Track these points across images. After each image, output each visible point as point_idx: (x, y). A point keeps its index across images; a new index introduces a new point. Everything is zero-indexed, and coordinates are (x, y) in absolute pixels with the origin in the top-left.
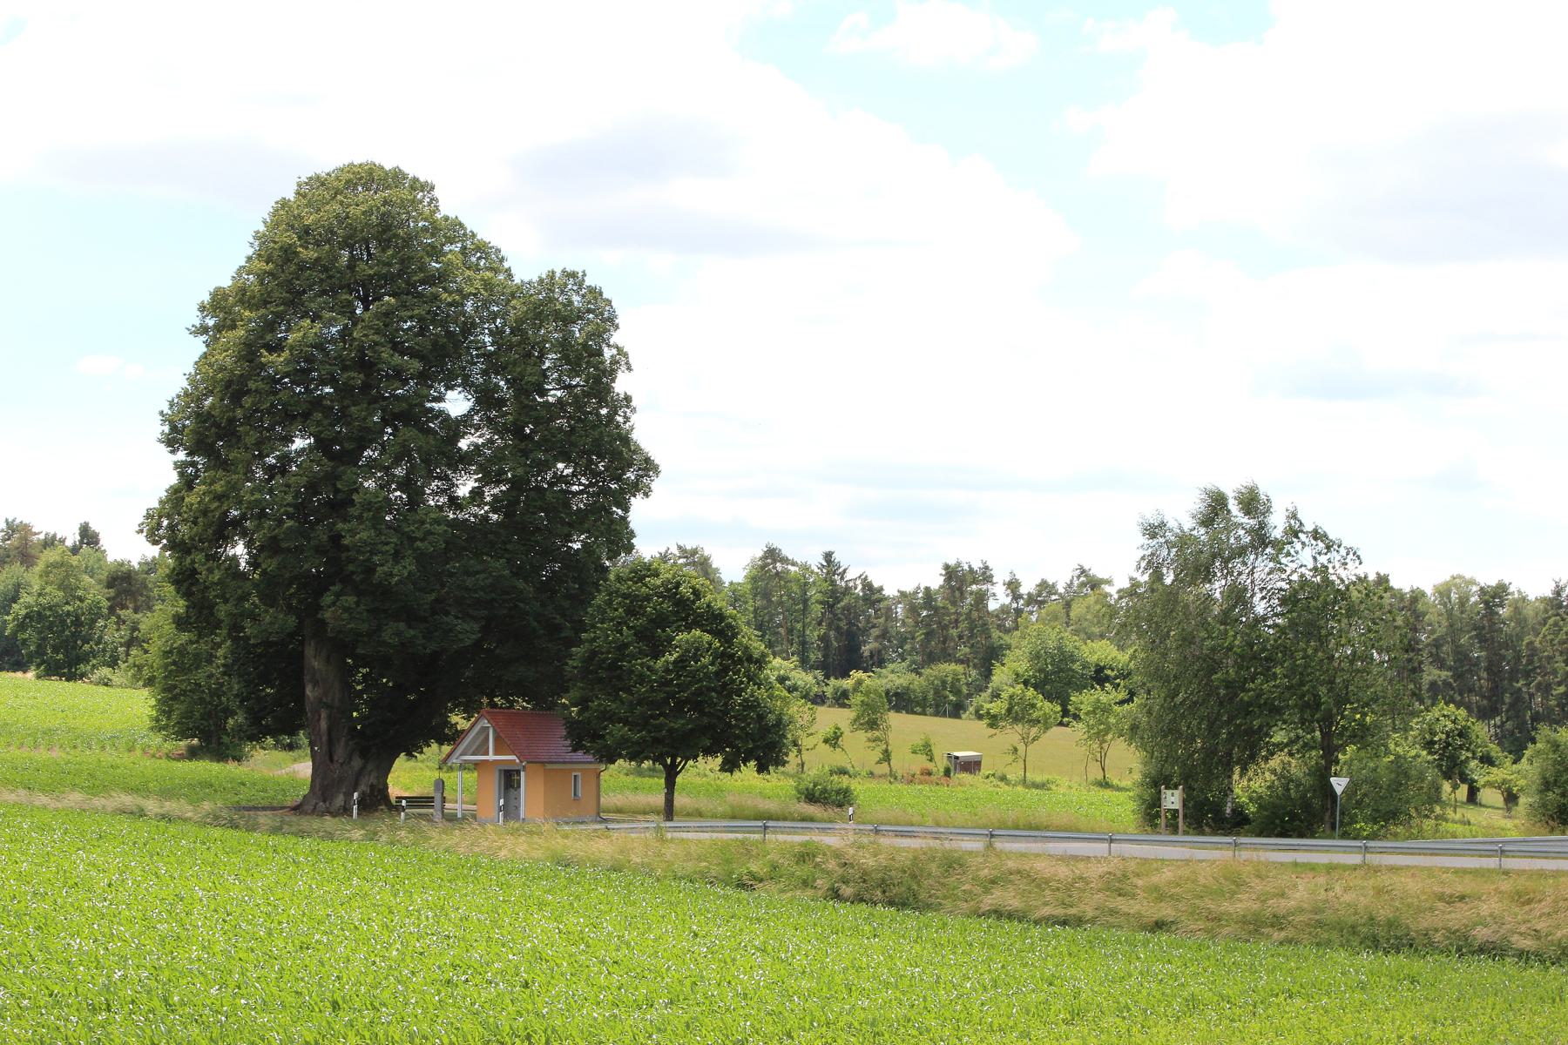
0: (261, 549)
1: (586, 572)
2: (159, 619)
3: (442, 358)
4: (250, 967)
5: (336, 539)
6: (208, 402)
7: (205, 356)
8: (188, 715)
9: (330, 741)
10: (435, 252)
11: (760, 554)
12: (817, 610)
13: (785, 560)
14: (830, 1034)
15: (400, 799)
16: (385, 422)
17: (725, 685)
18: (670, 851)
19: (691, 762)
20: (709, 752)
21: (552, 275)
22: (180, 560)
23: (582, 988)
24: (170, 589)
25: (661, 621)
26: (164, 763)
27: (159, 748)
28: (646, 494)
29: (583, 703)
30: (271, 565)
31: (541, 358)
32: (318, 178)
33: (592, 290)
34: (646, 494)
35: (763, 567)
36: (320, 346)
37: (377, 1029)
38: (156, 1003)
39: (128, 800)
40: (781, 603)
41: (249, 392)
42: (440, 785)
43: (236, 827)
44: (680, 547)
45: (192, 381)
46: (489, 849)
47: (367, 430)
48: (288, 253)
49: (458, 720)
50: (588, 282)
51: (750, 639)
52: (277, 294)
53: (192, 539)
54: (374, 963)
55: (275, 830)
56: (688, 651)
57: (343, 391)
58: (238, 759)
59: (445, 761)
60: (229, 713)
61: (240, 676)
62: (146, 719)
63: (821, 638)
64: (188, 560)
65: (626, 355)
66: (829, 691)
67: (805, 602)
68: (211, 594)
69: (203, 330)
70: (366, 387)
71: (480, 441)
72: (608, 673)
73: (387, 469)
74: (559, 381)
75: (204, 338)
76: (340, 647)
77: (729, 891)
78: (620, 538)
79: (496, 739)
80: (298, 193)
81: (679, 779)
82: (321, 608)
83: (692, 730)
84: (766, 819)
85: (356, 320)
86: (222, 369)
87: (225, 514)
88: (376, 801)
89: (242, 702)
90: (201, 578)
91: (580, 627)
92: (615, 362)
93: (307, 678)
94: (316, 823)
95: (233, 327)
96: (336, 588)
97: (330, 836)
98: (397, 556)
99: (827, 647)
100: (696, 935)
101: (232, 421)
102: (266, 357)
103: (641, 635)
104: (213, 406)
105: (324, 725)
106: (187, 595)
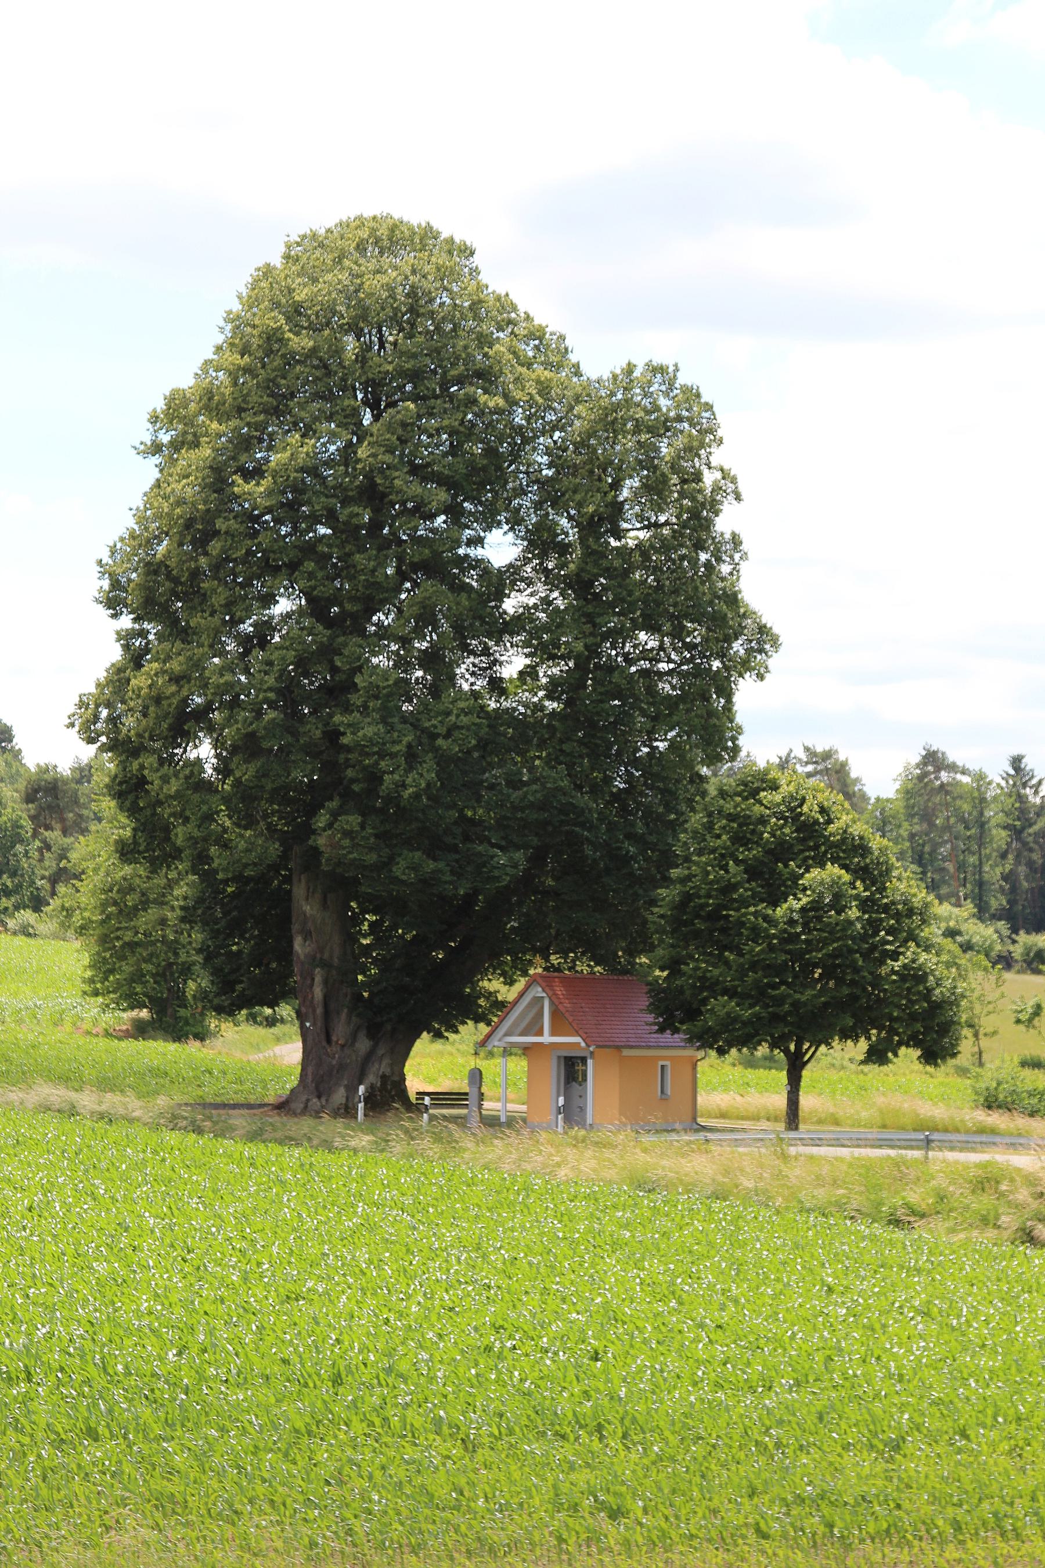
0: (234, 750)
1: (670, 780)
2: (96, 848)
3: (480, 483)
4: (219, 1324)
5: (333, 735)
6: (162, 549)
7: (158, 484)
8: (138, 977)
9: (327, 1013)
10: (484, 341)
11: (917, 759)
12: (1000, 837)
13: (952, 768)
14: (1021, 1434)
15: (421, 1095)
16: (402, 575)
17: (874, 948)
18: (795, 1173)
19: (823, 1048)
20: (848, 1034)
21: (630, 369)
22: (123, 765)
23: (673, 1363)
24: (108, 805)
25: (781, 852)
26: (103, 1043)
27: (95, 1021)
28: (761, 677)
29: (674, 966)
30: (246, 772)
31: (616, 485)
32: (314, 236)
33: (686, 390)
34: (761, 677)
35: (920, 778)
36: (313, 471)
37: (390, 1412)
38: (93, 1372)
39: (57, 1094)
40: (947, 828)
41: (216, 533)
42: (476, 1076)
43: (199, 1131)
44: (807, 749)
45: (141, 520)
46: (545, 1166)
47: (376, 585)
48: (272, 339)
49: (494, 985)
50: (682, 379)
51: (905, 884)
52: (255, 398)
53: (139, 735)
54: (387, 1321)
55: (254, 1136)
56: (821, 895)
57: (346, 532)
58: (201, 1037)
59: (483, 1043)
60: (186, 971)
61: (205, 923)
62: (78, 982)
63: (1005, 878)
64: (135, 765)
65: (734, 480)
66: (1017, 951)
67: (982, 825)
68: (165, 812)
69: (156, 448)
70: (375, 526)
71: (532, 601)
72: (707, 923)
73: (405, 642)
74: (640, 518)
75: (157, 459)
76: (340, 886)
77: (877, 1229)
78: (715, 733)
79: (555, 1014)
80: (287, 257)
81: (805, 1073)
82: (314, 832)
83: (826, 1005)
84: (928, 1135)
85: (362, 434)
86: (180, 502)
87: (185, 702)
88: (389, 1097)
89: (207, 959)
90: (153, 788)
91: (667, 859)
92: (717, 489)
93: (295, 927)
94: (305, 1125)
95: (196, 444)
96: (333, 804)
97: (328, 1146)
98: (412, 757)
99: (1014, 889)
100: (830, 1290)
101: (196, 574)
102: (241, 486)
103: (753, 872)
104: (168, 555)
105: (318, 992)
106: (133, 811)
